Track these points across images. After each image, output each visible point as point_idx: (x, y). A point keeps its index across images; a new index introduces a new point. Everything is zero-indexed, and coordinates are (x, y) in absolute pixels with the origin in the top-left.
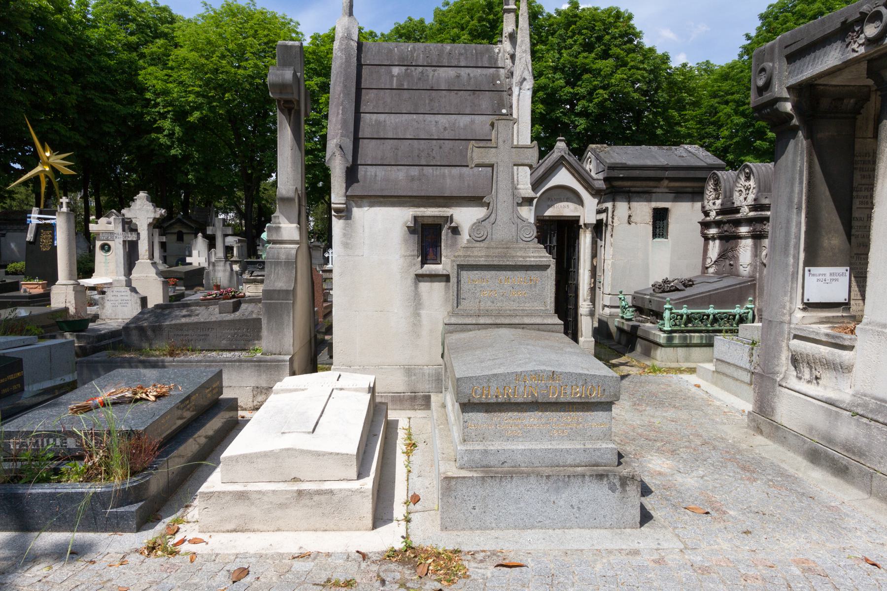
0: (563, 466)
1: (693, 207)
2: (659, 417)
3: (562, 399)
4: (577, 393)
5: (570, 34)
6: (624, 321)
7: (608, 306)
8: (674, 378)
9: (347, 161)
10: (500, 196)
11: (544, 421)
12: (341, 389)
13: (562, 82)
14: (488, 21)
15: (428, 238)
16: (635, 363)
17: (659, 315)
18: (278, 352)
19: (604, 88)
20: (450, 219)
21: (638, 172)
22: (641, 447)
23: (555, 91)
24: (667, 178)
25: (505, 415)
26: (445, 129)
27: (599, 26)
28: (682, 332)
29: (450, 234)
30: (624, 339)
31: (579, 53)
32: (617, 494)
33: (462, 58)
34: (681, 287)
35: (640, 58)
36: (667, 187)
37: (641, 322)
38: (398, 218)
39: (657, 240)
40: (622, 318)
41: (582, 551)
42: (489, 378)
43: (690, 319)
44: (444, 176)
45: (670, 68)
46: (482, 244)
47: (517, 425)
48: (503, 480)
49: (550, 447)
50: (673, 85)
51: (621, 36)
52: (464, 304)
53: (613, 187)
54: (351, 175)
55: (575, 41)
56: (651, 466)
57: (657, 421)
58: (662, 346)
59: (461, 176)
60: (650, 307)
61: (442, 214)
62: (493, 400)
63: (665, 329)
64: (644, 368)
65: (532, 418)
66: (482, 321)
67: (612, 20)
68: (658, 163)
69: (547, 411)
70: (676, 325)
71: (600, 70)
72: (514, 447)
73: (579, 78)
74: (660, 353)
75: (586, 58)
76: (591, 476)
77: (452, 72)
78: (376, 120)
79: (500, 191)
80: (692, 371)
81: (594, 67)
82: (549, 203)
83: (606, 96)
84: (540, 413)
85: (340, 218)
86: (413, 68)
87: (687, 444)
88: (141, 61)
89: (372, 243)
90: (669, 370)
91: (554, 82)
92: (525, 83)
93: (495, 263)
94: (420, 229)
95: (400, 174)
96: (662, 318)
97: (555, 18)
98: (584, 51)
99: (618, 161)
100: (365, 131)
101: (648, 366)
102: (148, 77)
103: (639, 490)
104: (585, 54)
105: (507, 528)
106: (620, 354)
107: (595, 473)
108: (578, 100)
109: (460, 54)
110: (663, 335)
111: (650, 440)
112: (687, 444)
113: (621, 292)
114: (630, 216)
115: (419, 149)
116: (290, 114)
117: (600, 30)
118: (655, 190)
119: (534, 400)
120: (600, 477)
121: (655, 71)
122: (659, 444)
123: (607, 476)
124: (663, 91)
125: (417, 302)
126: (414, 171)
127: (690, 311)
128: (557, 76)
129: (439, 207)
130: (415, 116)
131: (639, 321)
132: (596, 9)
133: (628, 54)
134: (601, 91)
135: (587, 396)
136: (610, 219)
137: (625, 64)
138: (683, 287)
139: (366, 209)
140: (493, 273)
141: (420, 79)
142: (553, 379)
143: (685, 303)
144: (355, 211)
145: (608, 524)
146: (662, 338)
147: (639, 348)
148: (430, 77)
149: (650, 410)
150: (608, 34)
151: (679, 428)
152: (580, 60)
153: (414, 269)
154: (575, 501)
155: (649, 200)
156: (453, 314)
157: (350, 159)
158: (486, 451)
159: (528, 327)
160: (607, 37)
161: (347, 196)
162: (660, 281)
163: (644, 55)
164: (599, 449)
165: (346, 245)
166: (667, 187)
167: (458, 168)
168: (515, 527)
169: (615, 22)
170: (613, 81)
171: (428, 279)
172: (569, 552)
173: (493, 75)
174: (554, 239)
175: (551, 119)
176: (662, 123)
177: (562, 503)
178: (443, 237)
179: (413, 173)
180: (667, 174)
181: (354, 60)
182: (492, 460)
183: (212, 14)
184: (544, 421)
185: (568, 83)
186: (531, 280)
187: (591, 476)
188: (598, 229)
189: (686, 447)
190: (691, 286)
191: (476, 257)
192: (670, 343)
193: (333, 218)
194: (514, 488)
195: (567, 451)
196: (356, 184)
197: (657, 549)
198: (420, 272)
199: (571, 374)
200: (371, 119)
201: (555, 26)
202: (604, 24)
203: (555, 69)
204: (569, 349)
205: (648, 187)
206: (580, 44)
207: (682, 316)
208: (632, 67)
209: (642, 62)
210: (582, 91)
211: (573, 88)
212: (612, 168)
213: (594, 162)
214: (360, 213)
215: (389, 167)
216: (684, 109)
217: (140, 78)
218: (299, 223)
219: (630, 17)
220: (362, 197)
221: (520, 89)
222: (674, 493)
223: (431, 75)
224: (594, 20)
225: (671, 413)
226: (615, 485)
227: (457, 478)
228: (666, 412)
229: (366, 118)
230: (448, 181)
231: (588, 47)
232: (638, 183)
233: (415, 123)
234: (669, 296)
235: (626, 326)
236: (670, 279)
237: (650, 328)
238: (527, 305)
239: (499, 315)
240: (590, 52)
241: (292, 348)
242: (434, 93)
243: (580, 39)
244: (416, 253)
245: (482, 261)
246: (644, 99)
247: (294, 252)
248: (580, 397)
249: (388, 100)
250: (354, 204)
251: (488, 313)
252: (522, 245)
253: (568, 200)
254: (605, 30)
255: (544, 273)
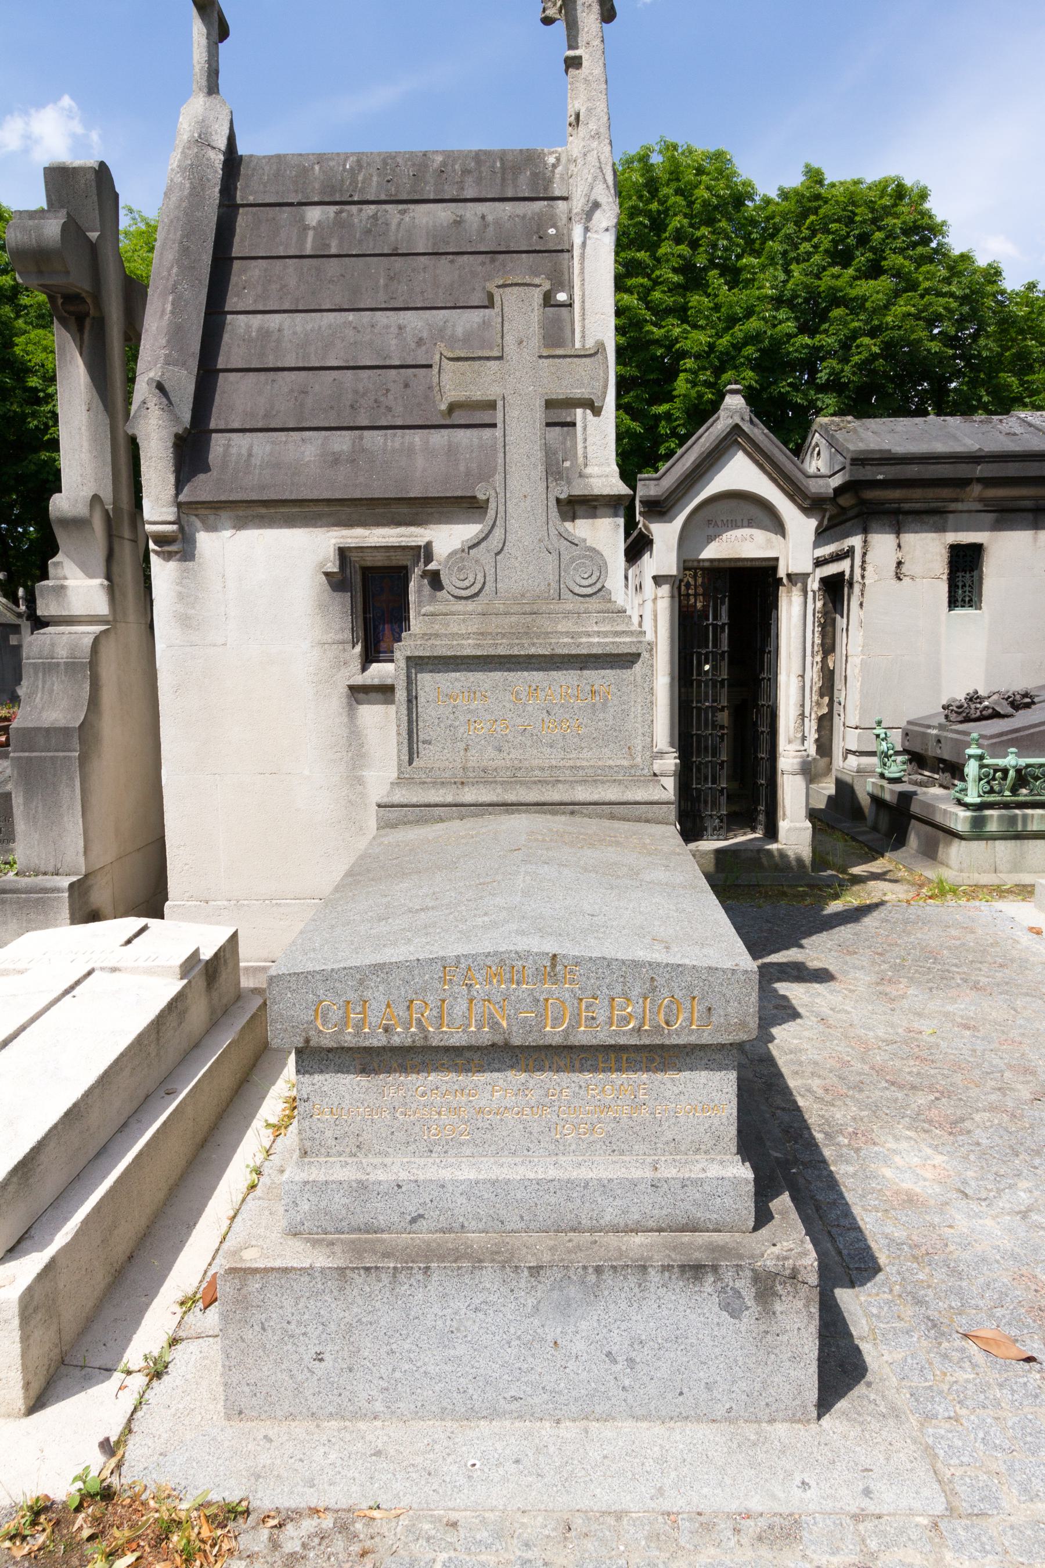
0: (592, 1230)
1: (1035, 540)
2: (933, 1016)
3: (583, 1036)
4: (626, 1020)
5: (806, 233)
6: (884, 783)
7: (854, 753)
8: (985, 910)
9: (176, 419)
10: (513, 483)
11: (533, 1097)
12: (114, 970)
13: (790, 326)
14: (648, 214)
15: (376, 599)
16: (903, 873)
17: (955, 770)
18: (51, 869)
19: (873, 333)
20: (426, 552)
21: (915, 468)
22: (875, 1109)
23: (777, 344)
24: (979, 480)
25: (415, 1081)
26: (420, 342)
27: (862, 213)
28: (1006, 806)
29: (427, 589)
30: (884, 823)
31: (824, 269)
32: (747, 1319)
33: (469, 180)
34: (1004, 708)
35: (943, 272)
36: (981, 500)
37: (921, 784)
38: (307, 551)
39: (959, 611)
40: (882, 776)
41: (619, 1516)
42: (363, 976)
43: (1022, 778)
44: (410, 451)
45: (1003, 292)
46: (470, 606)
47: (456, 1110)
48: (402, 1277)
49: (552, 1173)
50: (1006, 322)
51: (907, 232)
52: (428, 756)
53: (862, 502)
54: (190, 452)
55: (815, 247)
56: (888, 1172)
57: (926, 1026)
58: (961, 838)
59: (451, 451)
60: (938, 753)
61: (405, 541)
62: (379, 1040)
63: (968, 800)
64: (921, 886)
65: (498, 1089)
66: (469, 795)
67: (887, 201)
68: (958, 448)
69: (541, 1069)
70: (992, 791)
71: (864, 299)
72: (445, 1174)
73: (824, 316)
74: (956, 852)
75: (837, 277)
76: (666, 1268)
77: (443, 213)
78: (260, 329)
79: (512, 469)
80: (1025, 891)
81: (853, 293)
82: (711, 531)
83: (876, 350)
84: (523, 1076)
85: (168, 556)
86: (354, 209)
87: (994, 1097)
88: (20, 321)
89: (245, 614)
90: (974, 891)
91: (774, 326)
92: (598, 214)
93: (501, 651)
94: (358, 579)
95: (307, 450)
96: (963, 779)
97: (778, 204)
98: (833, 264)
99: (873, 446)
100: (232, 352)
101: (930, 881)
102: (30, 348)
103: (815, 1309)
104: (836, 270)
105: (418, 1415)
106: (874, 853)
107: (679, 1259)
108: (823, 359)
109: (466, 172)
110: (964, 814)
111: (901, 1087)
112: (994, 1097)
113: (879, 723)
114: (899, 564)
115: (356, 392)
116: (81, 329)
117: (864, 222)
118: (953, 506)
119: (499, 1039)
120: (695, 1272)
121: (972, 298)
122: (922, 1099)
123: (715, 1268)
124: (988, 337)
125: (354, 748)
126: (342, 442)
127: (1023, 762)
128: (782, 315)
129: (399, 524)
130: (351, 316)
131: (916, 783)
132: (857, 183)
133: (919, 266)
134: (866, 340)
135: (657, 1029)
136: (858, 571)
137: (913, 286)
138: (1010, 710)
139: (227, 533)
140: (497, 675)
141: (368, 232)
142: (554, 977)
143: (1012, 743)
144: (205, 541)
145: (720, 1410)
146: (960, 819)
147: (913, 841)
148: (393, 227)
149: (915, 995)
150: (880, 229)
151: (980, 1046)
152: (825, 283)
153: (345, 672)
154: (618, 1342)
155: (942, 529)
156: (402, 781)
157: (186, 417)
158: (363, 1186)
159: (585, 810)
160: (879, 235)
161: (179, 505)
162: (961, 697)
163: (951, 268)
164: (698, 1183)
165: (184, 622)
166: (981, 500)
167: (445, 432)
168: (443, 1414)
169: (895, 205)
170: (889, 319)
171: (380, 696)
172: (578, 1522)
173: (540, 215)
174: (724, 610)
175: (771, 398)
176: (986, 399)
177: (579, 1346)
178: (412, 597)
179: (337, 448)
180: (979, 471)
181: (214, 192)
182: (382, 1211)
183: (143, 228)
184: (533, 1097)
185: (803, 329)
186: (593, 693)
187: (666, 1268)
188: (835, 590)
189: (992, 1108)
190: (1028, 706)
191: (453, 636)
192: (978, 832)
193: (153, 558)
194: (436, 1302)
195: (605, 1186)
196: (202, 477)
197: (858, 1518)
198: (359, 679)
199: (609, 963)
200: (249, 327)
201: (777, 220)
202: (873, 210)
203: (778, 302)
204: (660, 875)
205: (937, 500)
206: (826, 251)
207: (1005, 771)
208: (927, 291)
209: (947, 281)
210: (827, 341)
211: (812, 336)
212: (860, 460)
213: (825, 454)
214: (217, 545)
215: (282, 435)
216: (1030, 369)
217: (17, 350)
218: (108, 577)
219: (923, 196)
220: (217, 507)
221: (587, 229)
222: (941, 1274)
223: (394, 222)
224: (854, 203)
225: (964, 1005)
226: (738, 1294)
227: (267, 1270)
228: (954, 1000)
229: (238, 326)
230: (420, 462)
231: (842, 257)
232: (917, 493)
233: (350, 333)
234: (976, 730)
235: (889, 793)
236: (982, 693)
237: (937, 797)
238: (586, 754)
239: (514, 781)
240: (845, 266)
241: (82, 860)
242: (398, 263)
243: (825, 241)
244: (348, 635)
245: (468, 648)
246: (951, 352)
247: (88, 641)
248: (638, 1030)
249: (292, 282)
250: (198, 524)
251: (485, 777)
252: (570, 604)
253: (750, 524)
254: (874, 221)
255: (626, 674)
